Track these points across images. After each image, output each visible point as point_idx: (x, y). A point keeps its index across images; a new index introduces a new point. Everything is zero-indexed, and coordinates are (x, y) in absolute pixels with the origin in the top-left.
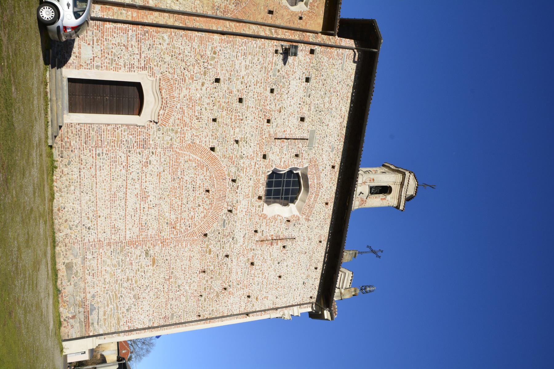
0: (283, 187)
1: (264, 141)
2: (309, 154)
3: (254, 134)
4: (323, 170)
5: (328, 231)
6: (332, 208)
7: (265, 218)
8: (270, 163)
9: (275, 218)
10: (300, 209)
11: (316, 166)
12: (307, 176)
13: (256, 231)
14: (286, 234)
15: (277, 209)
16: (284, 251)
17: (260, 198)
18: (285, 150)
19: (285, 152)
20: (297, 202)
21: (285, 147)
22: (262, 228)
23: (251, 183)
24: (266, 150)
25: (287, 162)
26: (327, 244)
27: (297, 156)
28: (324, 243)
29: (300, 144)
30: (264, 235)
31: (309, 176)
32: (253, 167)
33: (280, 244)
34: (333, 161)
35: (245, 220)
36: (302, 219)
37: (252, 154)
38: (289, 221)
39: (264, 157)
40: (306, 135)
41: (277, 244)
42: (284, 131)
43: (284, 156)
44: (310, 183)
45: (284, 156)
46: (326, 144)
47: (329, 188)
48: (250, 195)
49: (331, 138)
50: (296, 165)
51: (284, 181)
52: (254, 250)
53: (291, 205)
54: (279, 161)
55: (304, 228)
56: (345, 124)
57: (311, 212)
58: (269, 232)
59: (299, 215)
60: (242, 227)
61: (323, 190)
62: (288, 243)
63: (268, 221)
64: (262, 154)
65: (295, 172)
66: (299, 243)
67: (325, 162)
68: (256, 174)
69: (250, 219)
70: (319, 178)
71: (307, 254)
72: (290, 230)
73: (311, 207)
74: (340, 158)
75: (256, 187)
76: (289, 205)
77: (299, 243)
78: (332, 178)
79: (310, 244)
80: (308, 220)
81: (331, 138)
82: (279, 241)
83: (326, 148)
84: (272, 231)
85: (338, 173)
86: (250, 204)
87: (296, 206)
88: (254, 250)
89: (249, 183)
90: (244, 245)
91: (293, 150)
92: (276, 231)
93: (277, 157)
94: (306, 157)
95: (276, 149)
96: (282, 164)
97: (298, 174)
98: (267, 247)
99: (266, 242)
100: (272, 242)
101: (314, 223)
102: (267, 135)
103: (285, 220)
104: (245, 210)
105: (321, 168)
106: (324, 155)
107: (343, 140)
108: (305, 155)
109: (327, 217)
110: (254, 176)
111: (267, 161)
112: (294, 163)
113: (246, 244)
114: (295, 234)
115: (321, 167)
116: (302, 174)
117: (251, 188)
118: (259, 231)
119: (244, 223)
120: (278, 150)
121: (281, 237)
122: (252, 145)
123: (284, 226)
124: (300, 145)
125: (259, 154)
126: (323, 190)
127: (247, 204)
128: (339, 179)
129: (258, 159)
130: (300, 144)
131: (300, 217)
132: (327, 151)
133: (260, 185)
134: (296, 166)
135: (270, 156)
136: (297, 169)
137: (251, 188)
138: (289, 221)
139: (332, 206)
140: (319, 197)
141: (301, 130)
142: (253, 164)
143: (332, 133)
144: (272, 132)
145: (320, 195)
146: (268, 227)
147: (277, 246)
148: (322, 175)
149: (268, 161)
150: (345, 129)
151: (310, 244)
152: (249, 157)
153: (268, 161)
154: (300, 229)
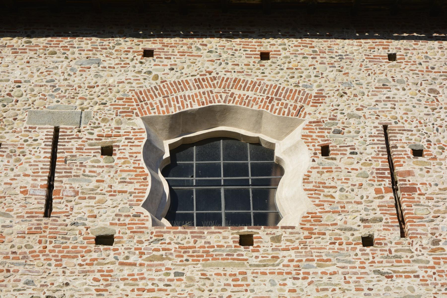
0: (218, 183)
1: (50, 247)
2: (104, 120)
3: (24, 279)
4: (156, 77)
5: (355, 42)
6: (280, 41)
7: (318, 219)
8: (127, 221)
9: (314, 189)
10: (286, 126)
11: (141, 97)
12: (175, 118)
13: (368, 241)
14: (372, 151)
15: (290, 197)
16: (434, 150)
17: (246, 241)
18: (84, 185)
19: (93, 184)
20: (265, 137)
21: (76, 185)
22: (353, 221)
23: (192, 271)
24: (80, 238)
25: (124, 175)
26: (397, 38)
27: (107, 151)
28: (394, 45)
29: (68, 146)
30: (379, 214)
31: (173, 111)
32: (136, 270)
33: (406, 164)
34: (130, 56)
35: (325, 279)
36: (311, 112)
37: (91, 277)
38: (325, 151)
39: (105, 240)
40: (44, 134)
41: (409, 173)
42: (25, 192)
43: (104, 186)
44: (196, 106)
45: (104, 186)
46: (76, 80)
47: (213, 56)
48: (236, 271)
49: (59, 71)
50: (134, 149)
51: (199, 183)
52: (436, 242)
53: (278, 153)
54: (119, 197)
55: (348, 106)
56: (18, 42)
57: (289, 94)
58: (368, 200)
59: (303, 125)
60: (352, 286)
61: (219, 69)
62: (402, 143)
63: (327, 207)
64: (93, 247)
65: (167, 154)
66: (399, 112)
67: (131, 75)
68: (161, 258)
69: (322, 262)
70: (180, 85)
71: (437, 87)
72: (356, 143)
73: (275, 95)
74: (121, 40)
75: (207, 255)
76: (279, 160)
77: (399, 112)
78: (183, 54)
79: (401, 82)
80: (319, 98)
81: (59, 71)
82: (397, 169)
83: (90, 77)
84: (362, 192)
85: (165, 40)
86: (267, 270)
87: (280, 138)
88: (436, 242)
89: (191, 279)
90: (421, 273)
91: (89, 163)
92: (361, 180)
93: (109, 203)
94: (114, 125)
95: (82, 209)
96: (130, 188)
97: (174, 149)
98: (423, 200)
99: (404, 206)
100: (405, 190)
101: (331, 80)
102: (33, 239)
103: (321, 159)
104: (290, 282)
105: (149, 84)
106: (111, 81)
107: (66, 41)
108: (105, 129)
109: (308, 51)
110: (168, 264)
111: (117, 231)
112: (131, 153)
113: (415, 267)
114: (371, 127)
115: (147, 83)
116: (172, 133)
117: (211, 272)
118: (365, 232)
119: (336, 279)
120: (84, 203)
121: (381, 163)
122: (61, 280)
123: (341, 161)
124: (74, 144)
125: (95, 255)
126: (219, 69)
127: (269, 277)
128: (186, 36)
129: (111, 258)
130: (69, 145)
131: (308, 119)
132: (96, 76)
133: (201, 242)
134: (141, 149)
135: (102, 225)
136: (150, 149)
137: (211, 272)
138: (325, 151)
139: (272, 41)
140: (241, 77)
141: (26, 149)
142: (127, 271)
143: (43, 69)
144: (24, 227)
145: (235, 76)
146: (349, 207)
147: (417, 172)
148: (172, 77)
149: (117, 229)
150: (34, 41)
151: (401, 82)
152: (102, 284)
153: (117, 229)
154: (351, 116)
